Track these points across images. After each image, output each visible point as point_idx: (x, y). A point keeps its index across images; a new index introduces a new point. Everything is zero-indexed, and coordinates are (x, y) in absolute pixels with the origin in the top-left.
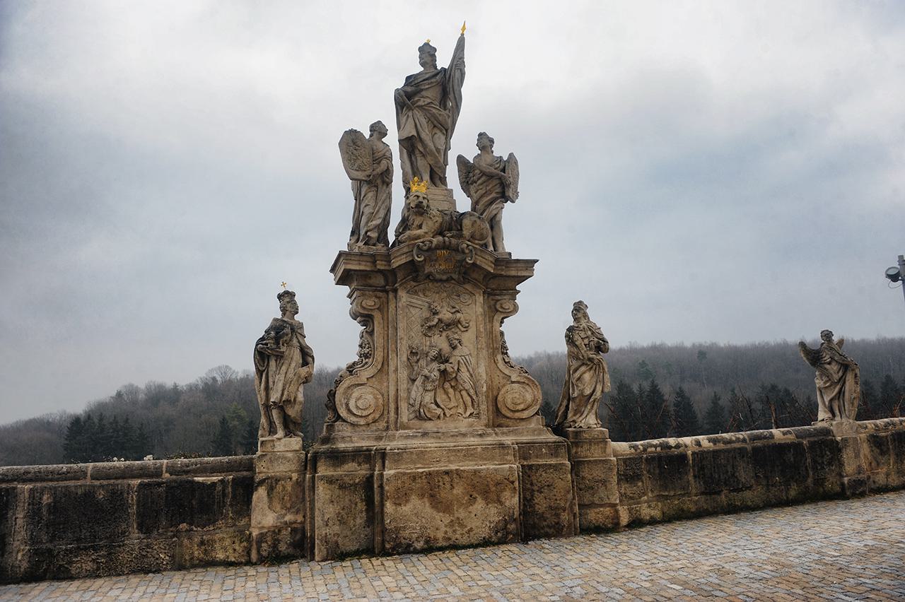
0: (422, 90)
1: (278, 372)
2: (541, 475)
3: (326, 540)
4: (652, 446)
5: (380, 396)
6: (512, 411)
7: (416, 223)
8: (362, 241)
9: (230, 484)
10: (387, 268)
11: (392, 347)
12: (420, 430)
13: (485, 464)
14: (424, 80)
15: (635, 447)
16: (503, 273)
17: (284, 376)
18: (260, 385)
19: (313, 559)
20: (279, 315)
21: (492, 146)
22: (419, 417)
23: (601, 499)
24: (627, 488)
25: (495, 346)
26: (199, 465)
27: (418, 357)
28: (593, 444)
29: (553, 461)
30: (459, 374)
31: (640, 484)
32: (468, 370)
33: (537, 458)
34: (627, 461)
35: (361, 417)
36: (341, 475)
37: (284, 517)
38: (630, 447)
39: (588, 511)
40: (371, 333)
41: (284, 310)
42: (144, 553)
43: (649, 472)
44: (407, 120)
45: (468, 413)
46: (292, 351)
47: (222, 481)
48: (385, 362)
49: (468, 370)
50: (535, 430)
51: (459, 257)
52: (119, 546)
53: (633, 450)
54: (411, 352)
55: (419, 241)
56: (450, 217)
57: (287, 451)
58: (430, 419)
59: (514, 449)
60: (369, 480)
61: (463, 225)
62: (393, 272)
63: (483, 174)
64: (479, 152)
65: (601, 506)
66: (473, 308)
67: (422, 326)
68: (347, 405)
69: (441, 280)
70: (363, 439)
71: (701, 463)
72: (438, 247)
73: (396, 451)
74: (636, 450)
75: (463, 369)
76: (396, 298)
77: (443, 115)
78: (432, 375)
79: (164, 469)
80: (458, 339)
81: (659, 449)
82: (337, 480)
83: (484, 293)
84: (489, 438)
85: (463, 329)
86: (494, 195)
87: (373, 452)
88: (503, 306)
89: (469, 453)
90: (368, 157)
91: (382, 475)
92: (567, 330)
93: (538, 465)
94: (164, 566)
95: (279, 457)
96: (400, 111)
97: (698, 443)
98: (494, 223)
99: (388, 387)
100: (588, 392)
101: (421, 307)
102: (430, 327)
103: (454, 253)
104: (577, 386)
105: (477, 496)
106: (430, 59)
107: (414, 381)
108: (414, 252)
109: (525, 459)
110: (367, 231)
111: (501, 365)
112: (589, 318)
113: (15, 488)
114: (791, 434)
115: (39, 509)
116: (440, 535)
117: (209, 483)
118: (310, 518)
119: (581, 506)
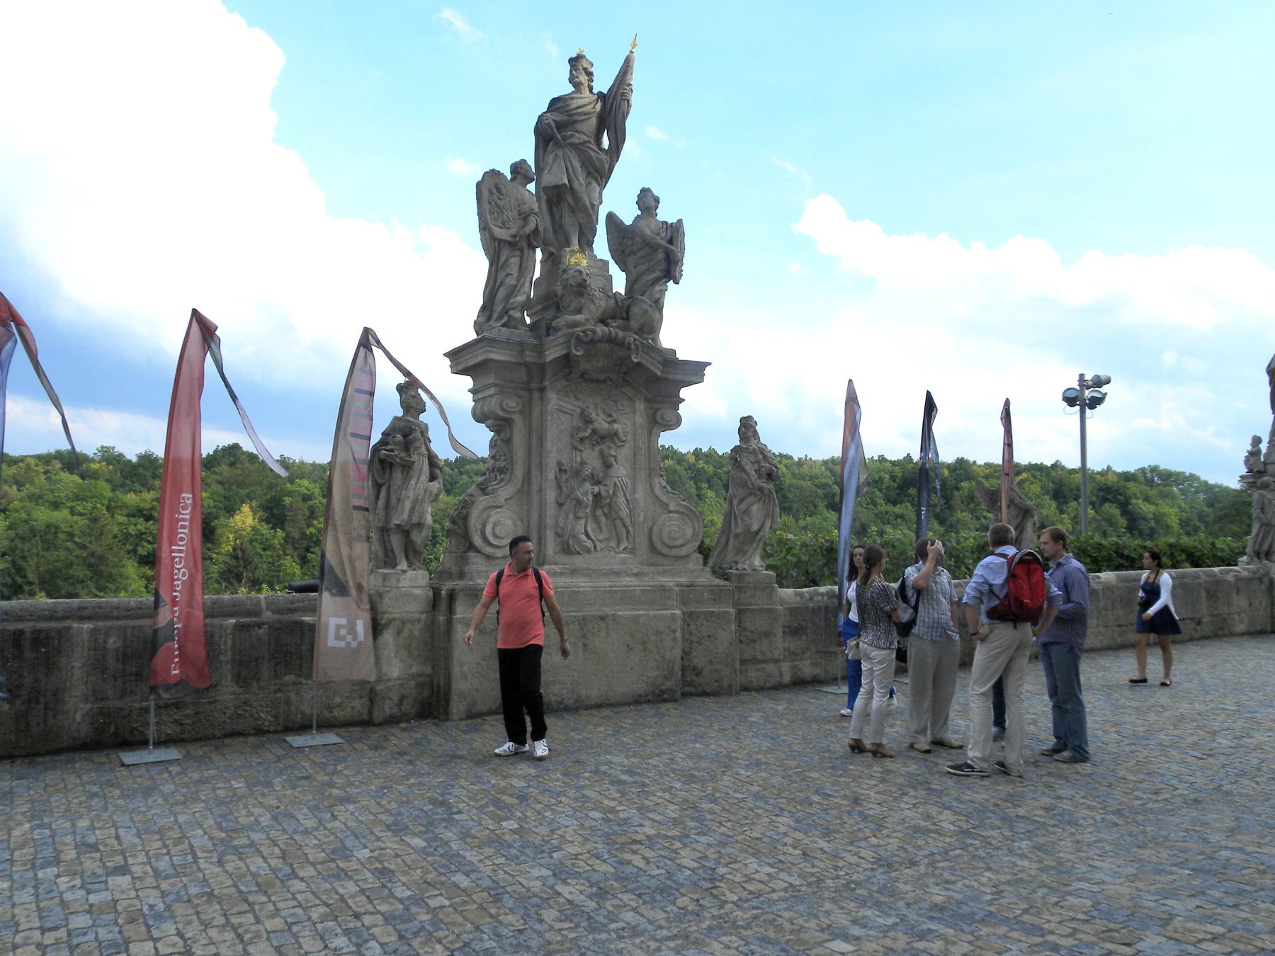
4: (818, 594)
7: (574, 305)
10: (537, 361)
11: (535, 461)
15: (801, 595)
19: (312, 628)
24: (793, 644)
34: (793, 611)
35: (498, 547)
40: (508, 442)
41: (406, 406)
42: (241, 712)
45: (622, 547)
52: (210, 703)
54: (561, 470)
62: (542, 367)
65: (763, 662)
67: (572, 437)
68: (483, 532)
69: (597, 381)
75: (620, 494)
76: (542, 399)
86: (658, 274)
89: (626, 597)
96: (541, 150)
100: (755, 527)
102: (582, 440)
104: (743, 520)
113: (69, 628)
115: (104, 655)
119: (743, 662)
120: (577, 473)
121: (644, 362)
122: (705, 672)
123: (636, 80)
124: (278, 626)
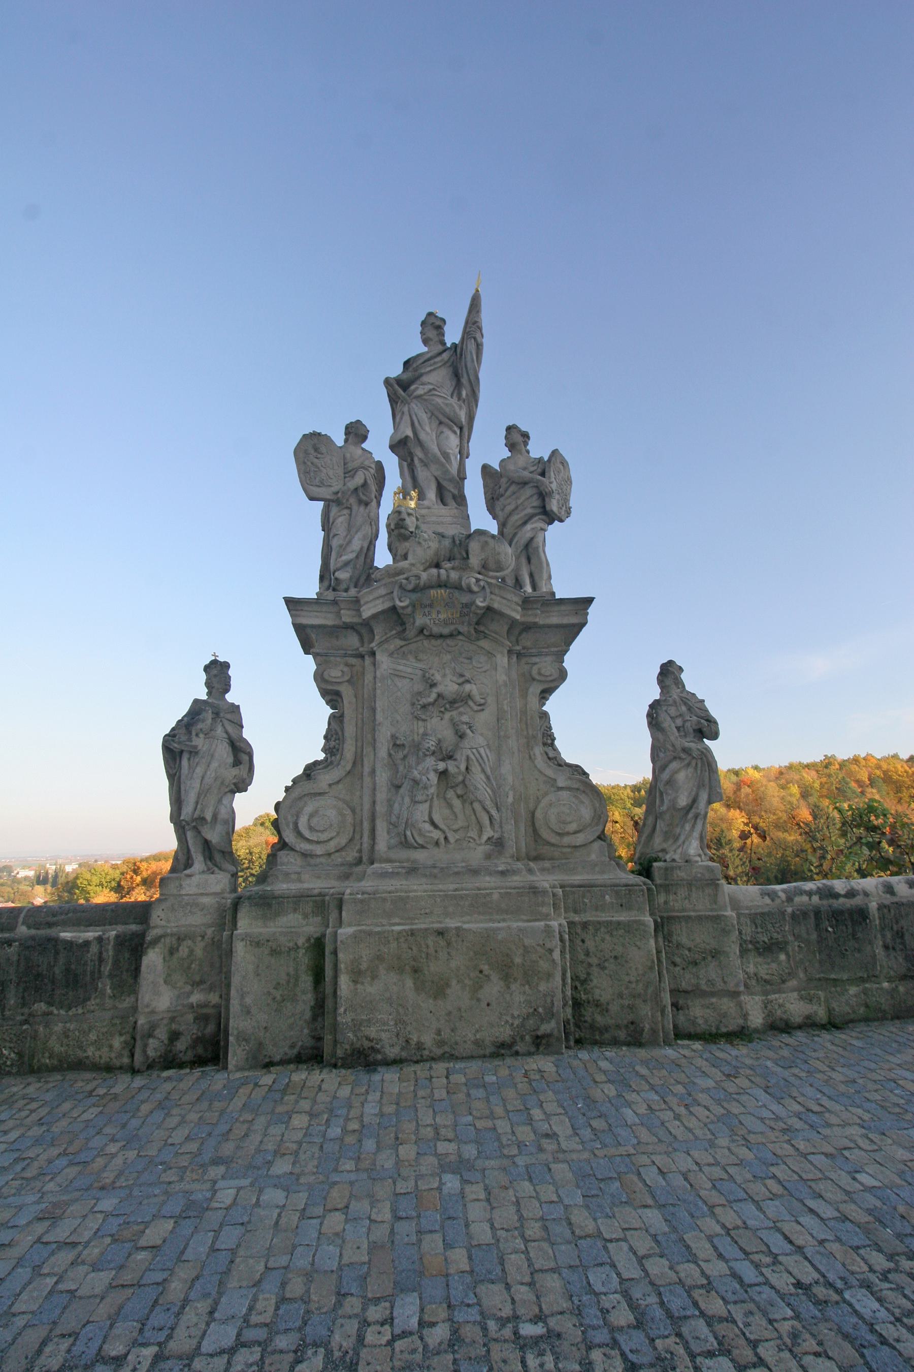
0: (421, 375)
2: (603, 940)
3: (243, 1038)
4: (802, 892)
5: (348, 812)
6: (559, 834)
9: (112, 943)
13: (504, 920)
14: (425, 362)
15: (773, 895)
16: (537, 620)
17: (199, 781)
21: (526, 444)
22: (405, 844)
23: (710, 982)
24: (757, 965)
25: (530, 733)
26: (70, 915)
27: (405, 752)
28: (694, 889)
29: (623, 917)
30: (468, 776)
31: (783, 957)
33: (597, 910)
34: (759, 919)
35: (318, 842)
36: (275, 933)
37: (188, 997)
38: (763, 894)
39: (690, 1003)
43: (797, 937)
45: (485, 838)
46: (214, 746)
47: (100, 939)
48: (358, 761)
49: (483, 771)
50: (596, 865)
51: (465, 598)
53: (767, 900)
54: (395, 745)
55: (402, 577)
56: (450, 540)
57: (202, 894)
58: (423, 847)
59: (554, 895)
60: (318, 946)
61: (470, 550)
62: (367, 624)
63: (512, 482)
65: (713, 994)
66: (493, 673)
67: (413, 704)
68: (296, 825)
69: (441, 636)
70: (319, 877)
71: (897, 923)
73: (359, 896)
74: (773, 900)
77: (451, 404)
78: (424, 777)
79: (21, 920)
80: (467, 723)
82: (268, 941)
83: (510, 652)
84: (516, 878)
85: (476, 708)
86: (529, 511)
87: (327, 898)
88: (543, 672)
89: (480, 904)
90: (336, 467)
91: (335, 934)
92: (650, 706)
93: (599, 923)
94: (7, 1069)
95: (187, 904)
97: (889, 889)
98: (531, 553)
99: (361, 797)
101: (412, 676)
102: (424, 707)
103: (457, 593)
105: (491, 972)
106: (435, 332)
107: (398, 787)
108: (395, 593)
109: (576, 912)
110: (344, 572)
111: (540, 762)
112: (684, 686)
116: (428, 1039)
117: (81, 941)
118: (565, 958)
120: (417, 746)
121: (496, 606)
122: (614, 1008)
123: (486, 318)
124: (30, 943)
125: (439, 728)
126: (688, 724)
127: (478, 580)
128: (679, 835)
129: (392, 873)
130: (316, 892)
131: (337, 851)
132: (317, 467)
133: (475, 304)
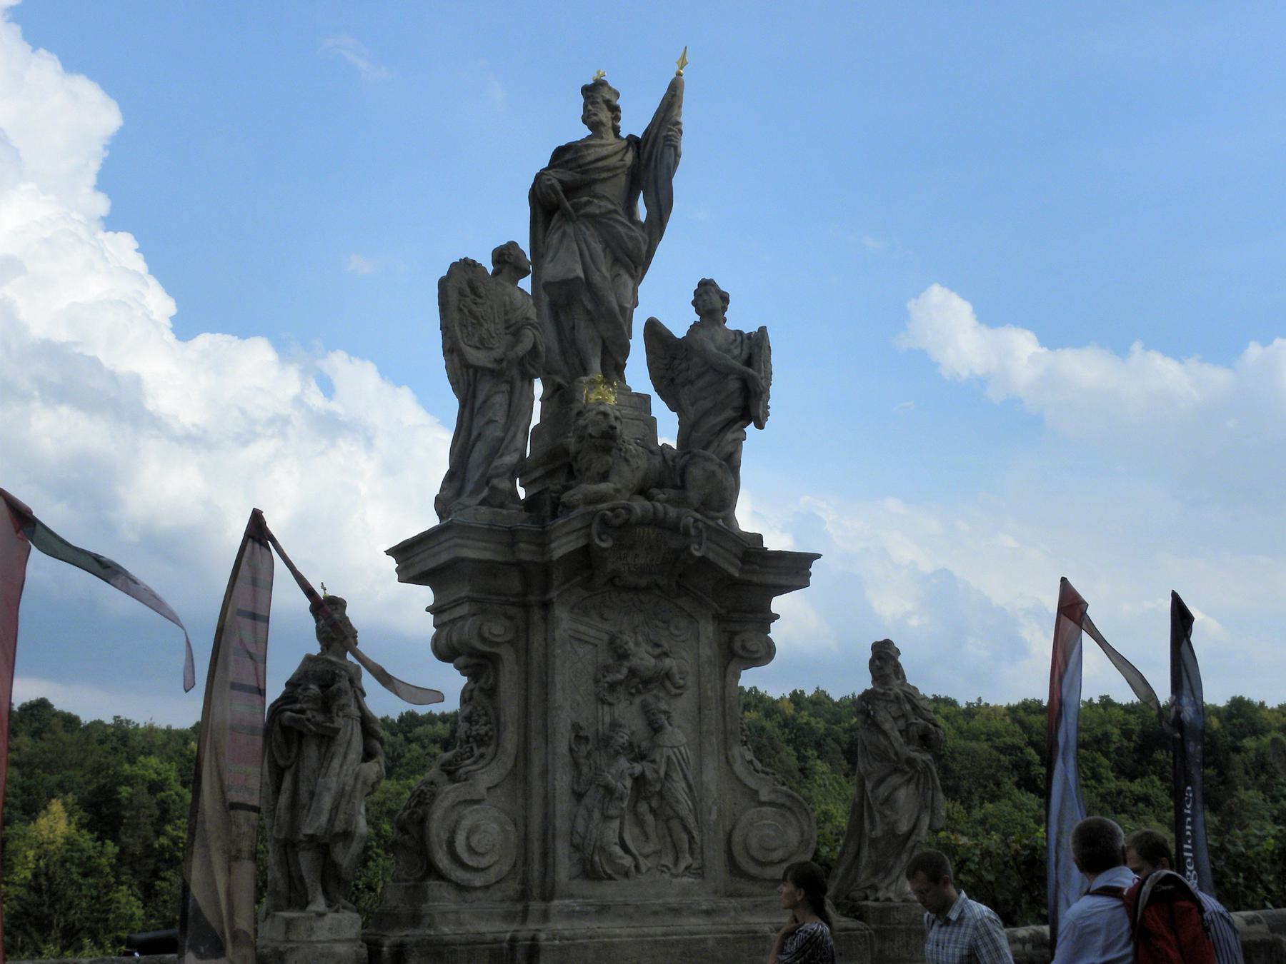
0: (594, 182)
1: (323, 771)
8: (476, 491)
10: (537, 559)
12: (591, 901)
18: (276, 799)
20: (315, 648)
21: (725, 309)
32: (685, 777)
44: (561, 242)
45: (682, 865)
49: (685, 777)
57: (335, 941)
58: (610, 878)
64: (698, 318)
67: (597, 681)
68: (451, 843)
69: (636, 589)
72: (642, 522)
73: (557, 942)
75: (677, 776)
81: (1029, 947)
85: (674, 691)
100: (904, 827)
101: (596, 642)
102: (612, 687)
104: (883, 816)
106: (609, 114)
114: (1260, 922)
121: (711, 556)
125: (628, 715)
126: (913, 729)
127: (696, 520)
128: (892, 867)
129: (580, 912)
130: (489, 937)
131: (497, 882)
132: (476, 318)
133: (1181, 619)
